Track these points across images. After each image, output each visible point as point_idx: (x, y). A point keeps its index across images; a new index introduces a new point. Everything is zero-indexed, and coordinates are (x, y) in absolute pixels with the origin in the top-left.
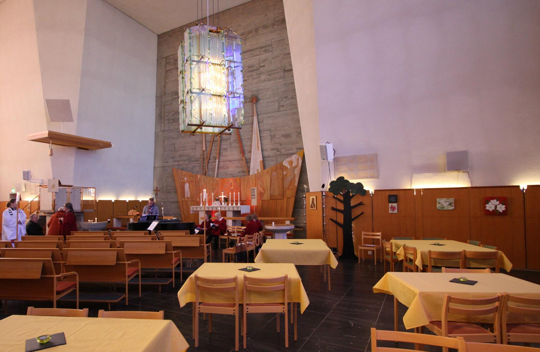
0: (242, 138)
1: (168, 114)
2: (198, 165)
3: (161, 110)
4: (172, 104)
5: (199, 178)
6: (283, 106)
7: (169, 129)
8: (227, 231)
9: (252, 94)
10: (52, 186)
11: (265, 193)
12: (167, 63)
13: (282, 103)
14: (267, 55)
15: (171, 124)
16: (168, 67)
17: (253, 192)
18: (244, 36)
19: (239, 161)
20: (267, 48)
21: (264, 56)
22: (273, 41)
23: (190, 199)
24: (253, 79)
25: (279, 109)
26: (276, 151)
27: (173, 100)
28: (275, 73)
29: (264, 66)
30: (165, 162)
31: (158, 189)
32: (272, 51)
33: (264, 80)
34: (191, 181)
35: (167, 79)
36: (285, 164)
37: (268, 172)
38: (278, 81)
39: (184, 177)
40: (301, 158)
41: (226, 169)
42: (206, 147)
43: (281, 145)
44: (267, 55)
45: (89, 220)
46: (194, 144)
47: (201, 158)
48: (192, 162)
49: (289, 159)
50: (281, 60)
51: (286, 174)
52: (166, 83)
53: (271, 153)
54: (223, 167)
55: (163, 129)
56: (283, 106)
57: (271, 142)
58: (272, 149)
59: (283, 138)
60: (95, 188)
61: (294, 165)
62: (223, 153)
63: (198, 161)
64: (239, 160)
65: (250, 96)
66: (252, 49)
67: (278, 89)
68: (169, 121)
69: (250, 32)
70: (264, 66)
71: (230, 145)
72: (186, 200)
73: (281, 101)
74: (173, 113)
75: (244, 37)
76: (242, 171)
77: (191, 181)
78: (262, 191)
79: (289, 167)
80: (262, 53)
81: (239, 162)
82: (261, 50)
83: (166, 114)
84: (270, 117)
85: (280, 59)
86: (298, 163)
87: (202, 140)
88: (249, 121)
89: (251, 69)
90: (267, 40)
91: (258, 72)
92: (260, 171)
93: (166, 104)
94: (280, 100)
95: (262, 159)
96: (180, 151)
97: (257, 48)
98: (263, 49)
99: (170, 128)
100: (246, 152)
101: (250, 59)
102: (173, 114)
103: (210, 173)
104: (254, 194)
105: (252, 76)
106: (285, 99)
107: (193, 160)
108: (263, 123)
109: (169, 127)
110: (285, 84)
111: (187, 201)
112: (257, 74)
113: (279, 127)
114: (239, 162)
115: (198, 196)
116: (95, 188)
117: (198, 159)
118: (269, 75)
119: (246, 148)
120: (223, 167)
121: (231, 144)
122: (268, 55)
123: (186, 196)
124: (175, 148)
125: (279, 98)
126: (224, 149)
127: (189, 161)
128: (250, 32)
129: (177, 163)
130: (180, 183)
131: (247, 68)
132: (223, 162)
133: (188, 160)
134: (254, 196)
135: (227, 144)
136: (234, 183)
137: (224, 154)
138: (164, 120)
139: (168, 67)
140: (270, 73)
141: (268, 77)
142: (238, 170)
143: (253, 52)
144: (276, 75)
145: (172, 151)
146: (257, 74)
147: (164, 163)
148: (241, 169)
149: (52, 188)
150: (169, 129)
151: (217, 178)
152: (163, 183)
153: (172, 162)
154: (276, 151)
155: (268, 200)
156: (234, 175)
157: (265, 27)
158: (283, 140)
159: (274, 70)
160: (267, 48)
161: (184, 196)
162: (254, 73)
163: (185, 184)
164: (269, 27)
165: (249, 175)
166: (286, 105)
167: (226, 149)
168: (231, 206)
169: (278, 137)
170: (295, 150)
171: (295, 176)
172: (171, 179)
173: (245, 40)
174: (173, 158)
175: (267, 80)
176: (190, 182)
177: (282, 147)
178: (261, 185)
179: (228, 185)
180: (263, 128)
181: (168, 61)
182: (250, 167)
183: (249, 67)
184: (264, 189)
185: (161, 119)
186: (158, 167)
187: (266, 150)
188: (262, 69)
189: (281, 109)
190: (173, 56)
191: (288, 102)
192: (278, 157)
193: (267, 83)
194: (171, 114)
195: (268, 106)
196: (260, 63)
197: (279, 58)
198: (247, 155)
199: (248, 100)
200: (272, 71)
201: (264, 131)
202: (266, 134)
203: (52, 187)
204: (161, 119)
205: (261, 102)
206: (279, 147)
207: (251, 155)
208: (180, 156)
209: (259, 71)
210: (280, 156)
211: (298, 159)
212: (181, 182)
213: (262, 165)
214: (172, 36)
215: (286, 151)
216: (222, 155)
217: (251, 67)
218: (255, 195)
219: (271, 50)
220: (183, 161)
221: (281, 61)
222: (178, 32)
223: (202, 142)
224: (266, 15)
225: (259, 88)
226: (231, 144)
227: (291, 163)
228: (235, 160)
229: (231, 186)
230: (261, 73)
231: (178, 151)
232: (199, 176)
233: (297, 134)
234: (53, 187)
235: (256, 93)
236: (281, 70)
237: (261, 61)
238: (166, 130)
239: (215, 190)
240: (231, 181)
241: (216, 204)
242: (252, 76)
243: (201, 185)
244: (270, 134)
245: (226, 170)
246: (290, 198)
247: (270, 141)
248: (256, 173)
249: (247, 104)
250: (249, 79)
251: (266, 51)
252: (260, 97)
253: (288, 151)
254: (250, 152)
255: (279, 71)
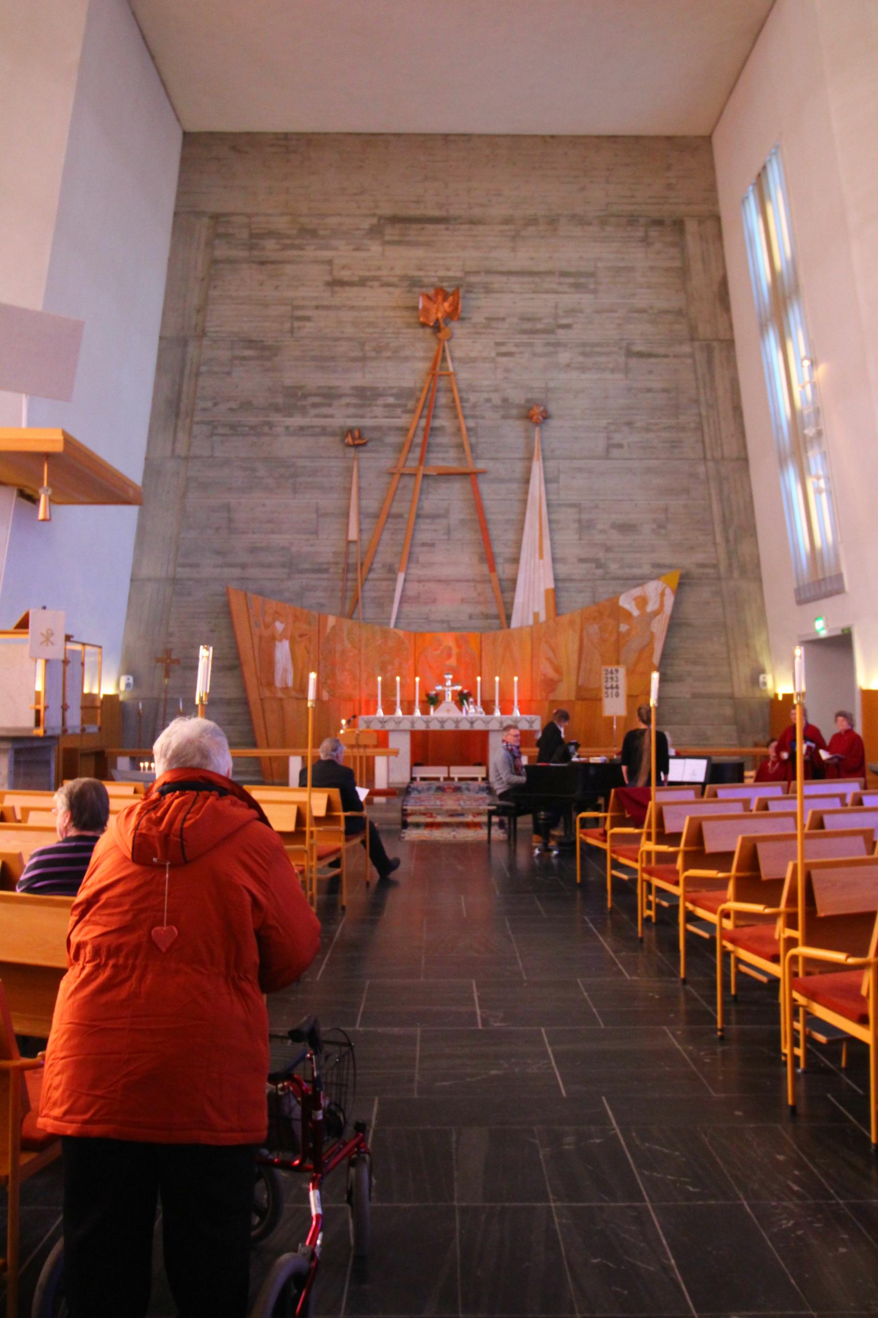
0: (489, 516)
1: (209, 404)
2: (324, 583)
3: (181, 386)
4: (229, 373)
5: (334, 628)
6: (620, 446)
7: (212, 457)
8: (148, 800)
9: (530, 396)
10: (42, 634)
11: (560, 681)
12: (218, 236)
13: (617, 438)
14: (581, 299)
15: (222, 442)
16: (222, 251)
17: (612, 678)
18: (511, 227)
19: (472, 584)
20: (582, 280)
21: (570, 299)
22: (600, 264)
23: (294, 694)
24: (535, 355)
25: (608, 452)
26: (593, 565)
27: (237, 362)
28: (600, 354)
29: (568, 326)
30: (183, 566)
31: (174, 656)
32: (595, 292)
33: (568, 366)
34: (301, 636)
35: (215, 287)
36: (626, 602)
37: (572, 623)
38: (608, 375)
39: (274, 620)
40: (673, 591)
41: (426, 603)
42: (360, 531)
43: (608, 549)
44: (581, 299)
45: (142, 765)
46: (314, 516)
47: (337, 563)
48: (301, 572)
49: (637, 592)
50: (618, 321)
51: (629, 632)
52: (206, 300)
53: (579, 570)
54: (416, 599)
55: (181, 449)
56: (620, 446)
57: (580, 539)
58: (582, 560)
59: (614, 531)
60: (100, 647)
61: (651, 607)
62: (423, 555)
63: (326, 571)
64: (474, 581)
65: (523, 402)
66: (535, 269)
67: (606, 397)
68: (215, 427)
69: (532, 221)
70: (568, 326)
71: (444, 534)
72: (280, 695)
73: (616, 431)
74: (233, 405)
75: (510, 230)
76: (482, 613)
77: (301, 636)
78: (551, 673)
79: (636, 613)
80: (565, 288)
81: (475, 586)
82: (563, 280)
83: (201, 404)
84: (580, 470)
85: (618, 318)
86: (662, 605)
87: (348, 508)
88: (514, 471)
89: (527, 326)
90: (581, 258)
91: (551, 338)
92: (543, 618)
93: (203, 369)
94: (612, 428)
95: (551, 585)
96: (254, 533)
97: (550, 273)
98: (571, 280)
99: (217, 454)
100: (499, 560)
101: (527, 296)
102: (231, 409)
103: (370, 612)
104: (614, 684)
105: (531, 345)
106: (626, 429)
107: (307, 566)
108: (558, 482)
109: (213, 448)
110: (630, 389)
111: (281, 699)
112: (548, 344)
113: (604, 500)
114: (475, 586)
115: (325, 683)
116: (100, 647)
117: (326, 566)
118: (583, 354)
119: (501, 550)
120: (416, 599)
121: (448, 531)
122: (586, 300)
123: (278, 683)
124: (230, 520)
125: (609, 424)
126: (424, 545)
127: (286, 570)
128: (532, 221)
129: (237, 572)
130: (256, 640)
131: (515, 320)
132: (419, 581)
133: (283, 565)
134: (615, 691)
135: (435, 530)
136: (459, 647)
137: (422, 558)
138: (188, 420)
139: (222, 251)
140: (588, 349)
141: (581, 359)
142: (468, 609)
143: (537, 280)
144: (602, 359)
145: (217, 529)
146: (548, 344)
147: (179, 569)
148: (480, 609)
149: (42, 643)
150: (212, 457)
151: (396, 630)
152: (170, 635)
153: (218, 566)
154: (593, 565)
155: (570, 701)
156: (453, 625)
157: (580, 220)
158: (615, 537)
159: (598, 345)
160: (582, 280)
161: (271, 684)
162: (539, 341)
163: (277, 643)
164: (590, 224)
165: (509, 626)
166: (629, 445)
167: (433, 545)
168: (419, 718)
169: (600, 527)
170: (646, 570)
171: (651, 642)
172: (210, 623)
173: (514, 238)
174: (219, 553)
175: (578, 368)
176: (298, 639)
177: (610, 555)
178: (548, 659)
179: (437, 653)
180: (556, 497)
181: (221, 230)
182: (512, 604)
183: (524, 319)
184: (557, 670)
185: (177, 415)
186: (149, 580)
187: (563, 560)
188: (561, 334)
189: (615, 452)
190: (245, 220)
191: (635, 438)
192: (598, 583)
193: (574, 374)
194: (223, 407)
195: (576, 438)
196: (556, 316)
197: (616, 315)
198: (504, 570)
199: (514, 412)
200: (594, 345)
201: (559, 505)
202: (567, 516)
203: (43, 639)
204: (177, 415)
205: (553, 423)
206: (601, 555)
207: (517, 569)
208: (253, 550)
209: (553, 336)
210: (604, 579)
211: (663, 594)
212: (261, 637)
213: (551, 601)
214: (246, 153)
215: (622, 567)
216: (418, 562)
217: (529, 320)
218: (617, 687)
219: (592, 287)
220: (262, 565)
221: (619, 325)
222: (272, 145)
223: (347, 515)
224: (583, 189)
225: (552, 384)
226: (448, 531)
227: (642, 602)
228: (459, 581)
229: (449, 656)
230: (557, 344)
231: (246, 533)
232: (331, 621)
233: (655, 526)
234: (47, 639)
235: (543, 396)
236: (621, 348)
237: (560, 312)
238: (196, 457)
239: (390, 667)
240: (449, 641)
241: (448, 711)
242: (531, 345)
243: (339, 648)
244: (576, 517)
245: (426, 609)
246: (637, 696)
247: (577, 537)
248: (531, 622)
249: (511, 422)
250: (521, 353)
251: (577, 287)
252: (552, 408)
253: (627, 570)
254: (516, 560)
255: (615, 349)
